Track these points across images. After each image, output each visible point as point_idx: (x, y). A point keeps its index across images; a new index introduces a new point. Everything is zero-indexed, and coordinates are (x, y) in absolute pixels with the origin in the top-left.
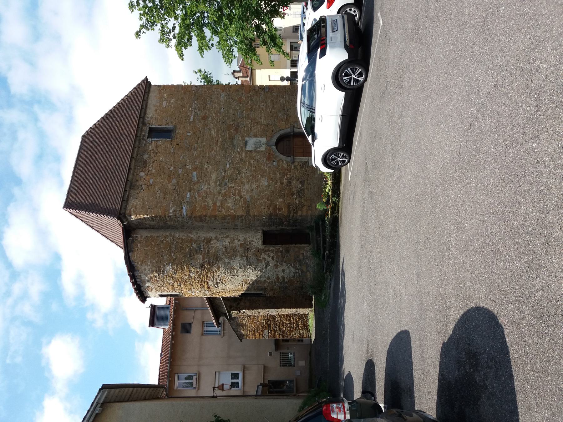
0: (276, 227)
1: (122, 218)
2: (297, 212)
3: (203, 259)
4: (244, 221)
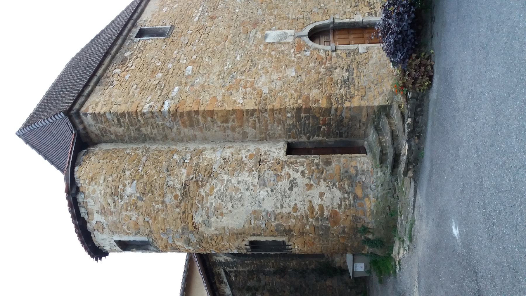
0: (309, 138)
1: (74, 117)
2: (343, 103)
3: (188, 175)
4: (258, 125)
